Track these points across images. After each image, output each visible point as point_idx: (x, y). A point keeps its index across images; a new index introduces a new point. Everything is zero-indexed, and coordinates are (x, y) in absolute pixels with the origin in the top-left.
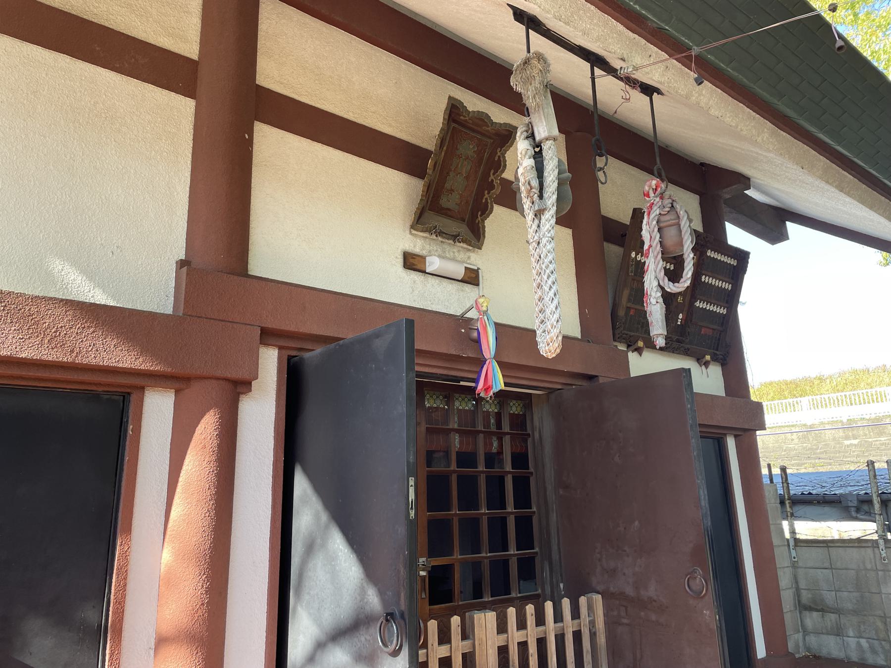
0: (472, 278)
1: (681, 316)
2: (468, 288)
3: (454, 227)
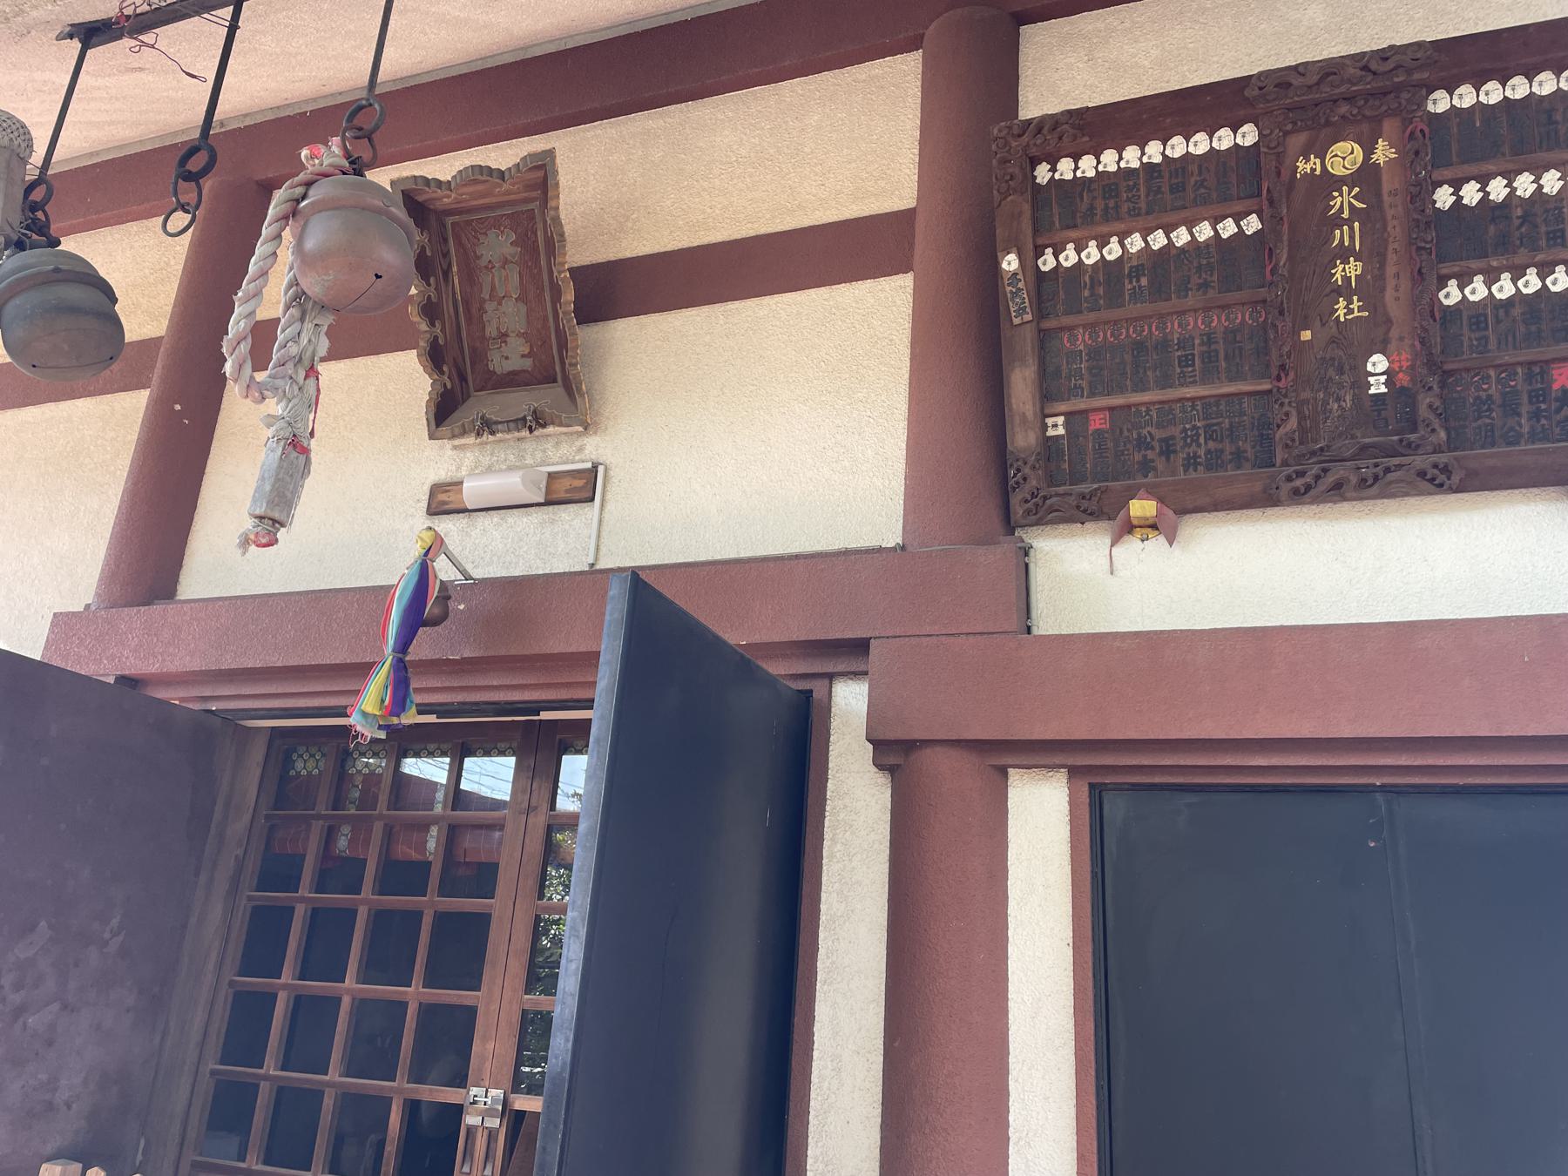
0: (575, 489)
1: (1378, 363)
2: (566, 513)
3: (521, 401)
